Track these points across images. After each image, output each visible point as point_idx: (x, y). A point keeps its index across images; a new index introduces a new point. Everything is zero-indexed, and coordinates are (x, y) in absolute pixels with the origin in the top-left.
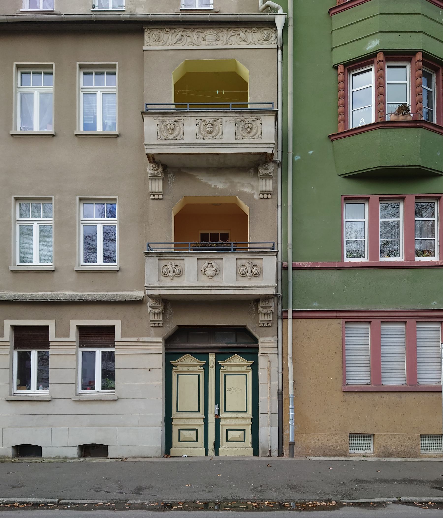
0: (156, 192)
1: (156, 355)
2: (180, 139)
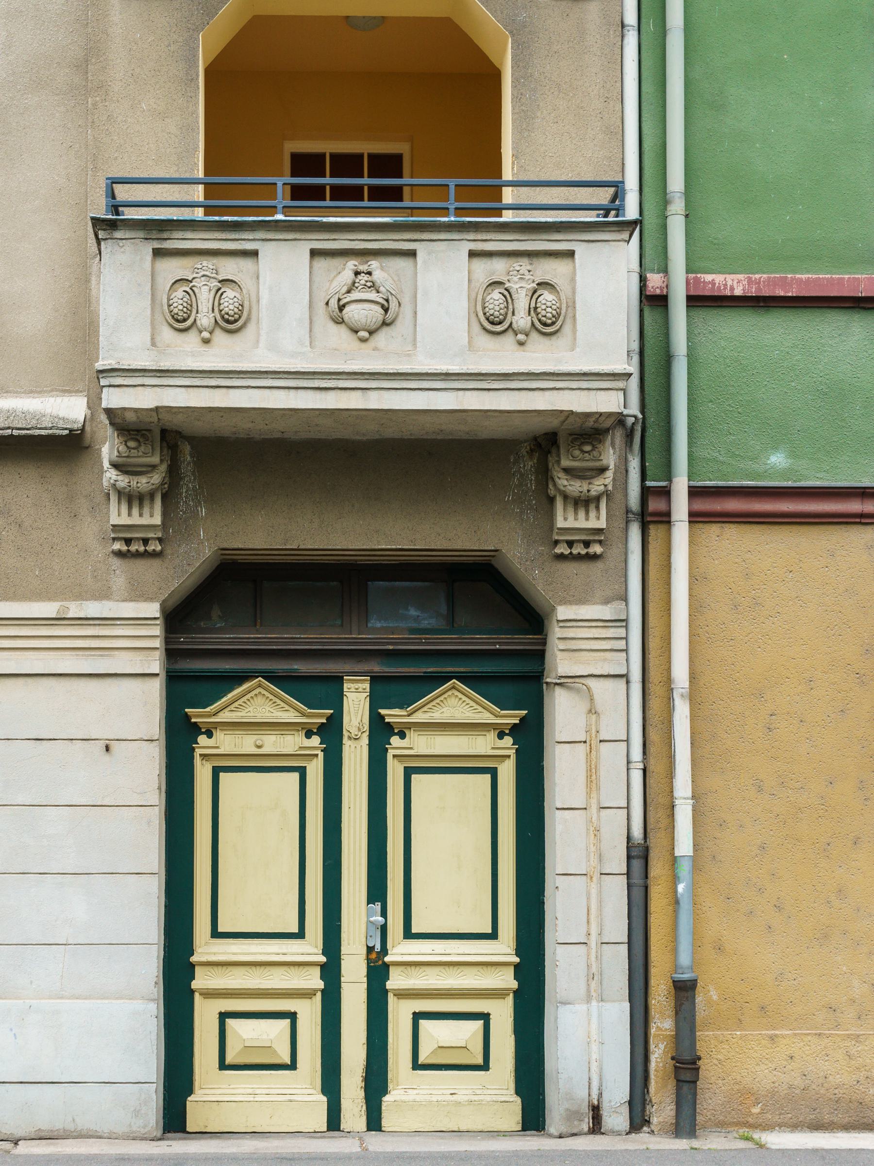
1: (83, 682)
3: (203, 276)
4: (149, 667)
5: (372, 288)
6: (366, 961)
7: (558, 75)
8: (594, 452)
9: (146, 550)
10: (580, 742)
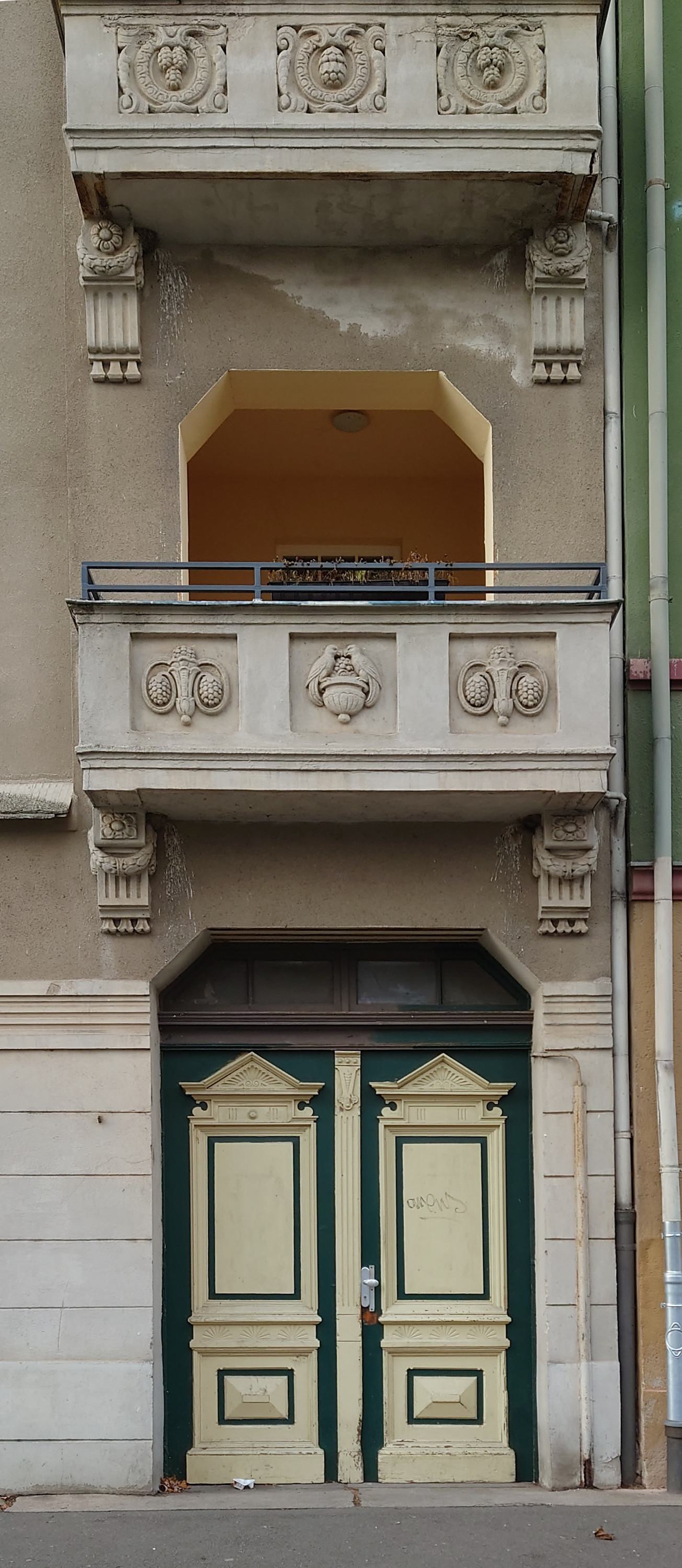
0: (112, 352)
2: (213, 109)
3: (182, 660)
4: (140, 1043)
5: (353, 672)
6: (361, 1321)
7: (540, 463)
8: (578, 832)
9: (134, 930)
10: (567, 1112)
